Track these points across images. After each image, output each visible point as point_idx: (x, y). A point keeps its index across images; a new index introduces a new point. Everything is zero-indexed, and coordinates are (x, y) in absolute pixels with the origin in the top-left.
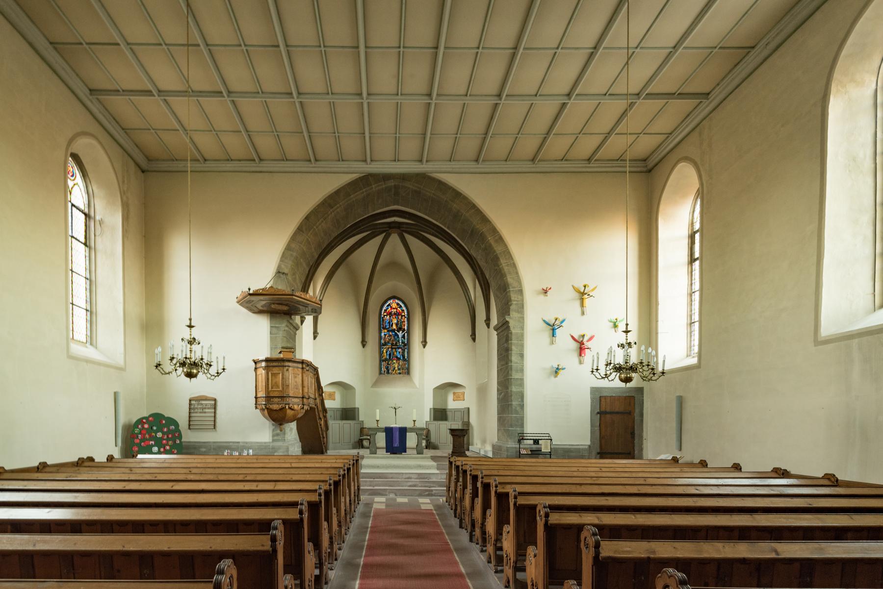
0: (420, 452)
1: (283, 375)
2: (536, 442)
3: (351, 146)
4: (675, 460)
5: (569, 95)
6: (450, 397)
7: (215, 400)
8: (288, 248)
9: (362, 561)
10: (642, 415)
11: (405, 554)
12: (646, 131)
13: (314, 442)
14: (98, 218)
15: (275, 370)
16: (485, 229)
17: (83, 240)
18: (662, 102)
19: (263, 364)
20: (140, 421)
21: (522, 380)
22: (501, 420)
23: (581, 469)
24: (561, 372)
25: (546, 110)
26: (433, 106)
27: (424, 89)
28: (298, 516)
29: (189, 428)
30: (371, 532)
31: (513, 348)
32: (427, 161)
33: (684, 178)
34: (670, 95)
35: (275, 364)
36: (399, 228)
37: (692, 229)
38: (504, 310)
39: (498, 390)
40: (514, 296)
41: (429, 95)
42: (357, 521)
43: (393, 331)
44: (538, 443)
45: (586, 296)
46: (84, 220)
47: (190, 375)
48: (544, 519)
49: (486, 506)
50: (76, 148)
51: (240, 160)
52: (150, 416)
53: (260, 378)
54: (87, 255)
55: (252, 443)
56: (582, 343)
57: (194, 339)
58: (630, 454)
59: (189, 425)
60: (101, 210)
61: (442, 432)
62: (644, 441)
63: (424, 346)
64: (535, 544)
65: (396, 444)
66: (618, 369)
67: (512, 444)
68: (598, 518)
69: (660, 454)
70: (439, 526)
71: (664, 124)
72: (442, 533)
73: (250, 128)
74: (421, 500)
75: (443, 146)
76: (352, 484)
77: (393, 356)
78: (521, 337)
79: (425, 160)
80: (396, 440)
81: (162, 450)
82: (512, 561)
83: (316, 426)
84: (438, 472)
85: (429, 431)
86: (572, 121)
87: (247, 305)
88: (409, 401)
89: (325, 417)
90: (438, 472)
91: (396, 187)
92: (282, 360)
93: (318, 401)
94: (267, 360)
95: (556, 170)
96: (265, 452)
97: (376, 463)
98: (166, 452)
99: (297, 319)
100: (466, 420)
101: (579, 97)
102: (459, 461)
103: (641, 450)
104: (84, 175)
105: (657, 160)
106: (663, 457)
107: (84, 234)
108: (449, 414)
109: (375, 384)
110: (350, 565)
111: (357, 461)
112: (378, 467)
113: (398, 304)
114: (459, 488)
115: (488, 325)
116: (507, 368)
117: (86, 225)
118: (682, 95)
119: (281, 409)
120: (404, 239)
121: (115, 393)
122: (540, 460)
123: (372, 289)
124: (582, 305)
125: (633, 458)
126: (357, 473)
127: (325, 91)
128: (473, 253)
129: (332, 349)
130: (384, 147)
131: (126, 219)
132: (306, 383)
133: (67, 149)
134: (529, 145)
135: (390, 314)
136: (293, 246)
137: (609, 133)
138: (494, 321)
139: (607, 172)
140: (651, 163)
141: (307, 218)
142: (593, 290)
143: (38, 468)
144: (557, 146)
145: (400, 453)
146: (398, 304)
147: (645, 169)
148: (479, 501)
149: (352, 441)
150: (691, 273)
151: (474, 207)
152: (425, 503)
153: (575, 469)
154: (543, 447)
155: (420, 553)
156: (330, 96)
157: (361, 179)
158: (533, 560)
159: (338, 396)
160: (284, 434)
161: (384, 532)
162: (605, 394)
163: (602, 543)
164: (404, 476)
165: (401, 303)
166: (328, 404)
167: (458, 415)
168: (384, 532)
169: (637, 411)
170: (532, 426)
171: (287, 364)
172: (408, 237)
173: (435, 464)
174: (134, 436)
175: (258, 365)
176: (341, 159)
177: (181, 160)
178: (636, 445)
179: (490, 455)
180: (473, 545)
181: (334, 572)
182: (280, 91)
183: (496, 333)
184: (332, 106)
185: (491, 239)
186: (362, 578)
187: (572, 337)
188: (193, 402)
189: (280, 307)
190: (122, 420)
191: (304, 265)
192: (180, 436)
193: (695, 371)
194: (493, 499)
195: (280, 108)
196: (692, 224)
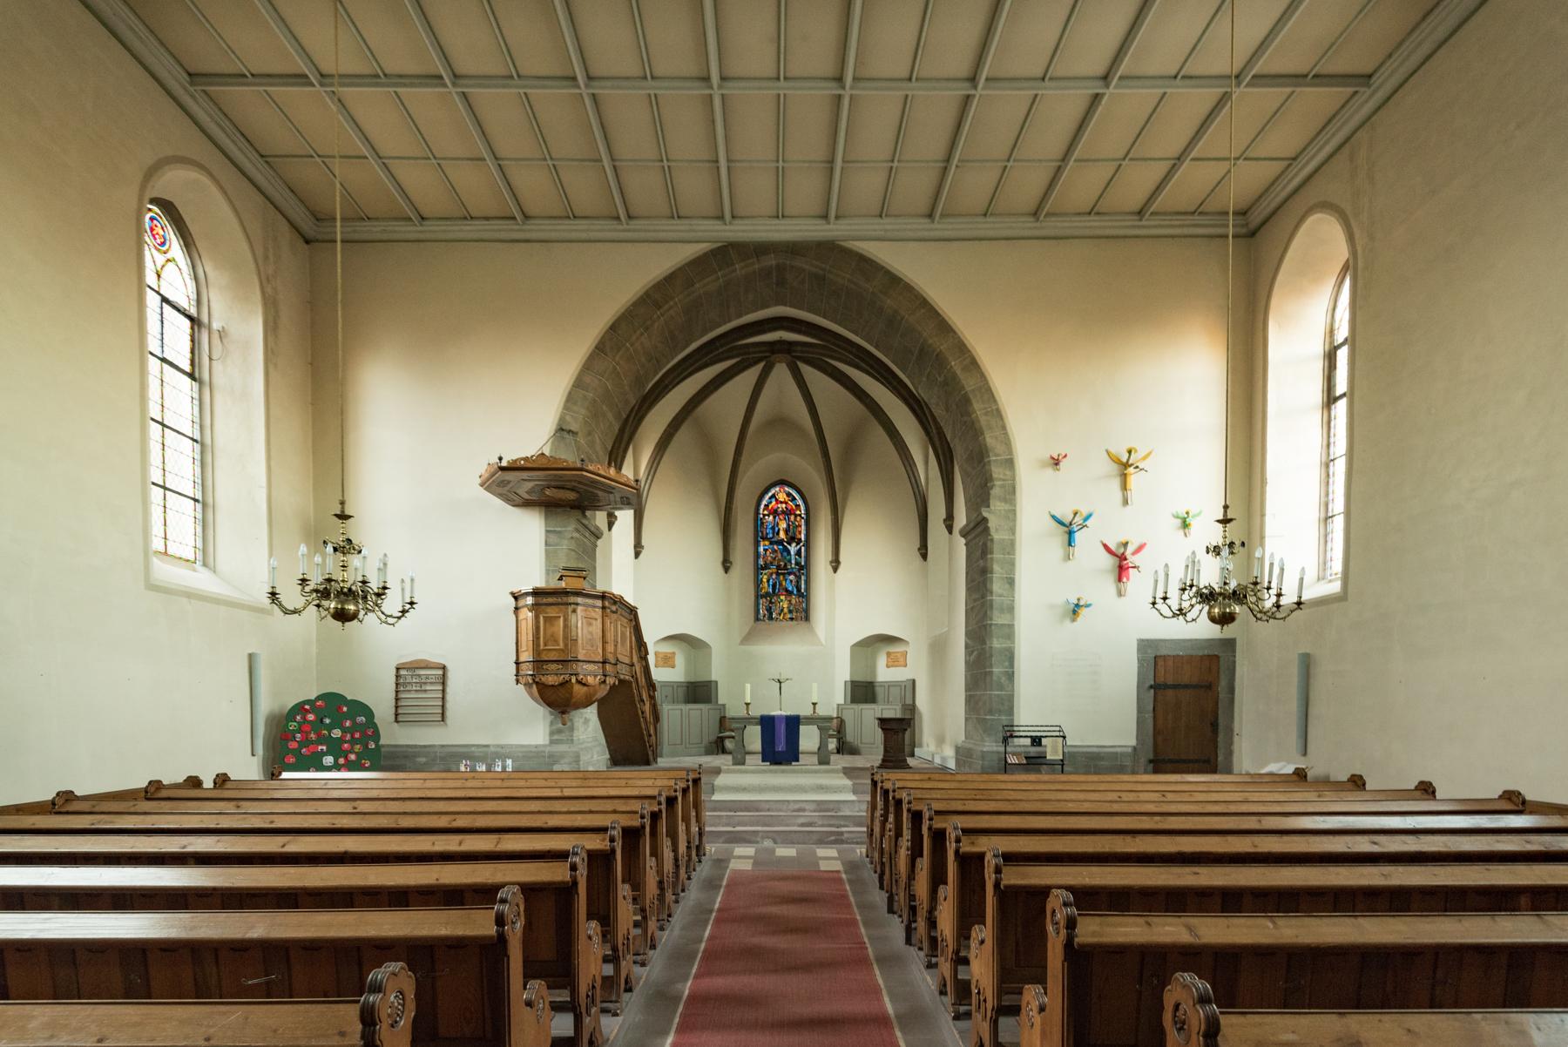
0: (824, 761)
1: (566, 620)
2: (1036, 741)
3: (694, 188)
4: (1300, 775)
5: (1106, 78)
6: (882, 661)
7: (444, 668)
8: (578, 384)
9: (687, 989)
10: (1231, 690)
11: (776, 971)
12: (1249, 154)
13: (631, 741)
14: (216, 325)
15: (552, 612)
16: (943, 346)
17: (188, 368)
18: (1278, 93)
19: (530, 600)
20: (300, 708)
21: (1011, 626)
22: (972, 702)
23: (1125, 796)
24: (1083, 612)
25: (1064, 106)
26: (846, 102)
27: (827, 67)
28: (492, 930)
29: (397, 721)
30: (718, 921)
31: (996, 567)
32: (837, 217)
33: (1322, 239)
34: (1297, 79)
35: (550, 600)
36: (789, 352)
37: (1332, 342)
38: (980, 496)
39: (967, 647)
40: (997, 472)
41: (840, 79)
42: (693, 895)
43: (780, 542)
44: (1040, 744)
45: (1131, 470)
46: (189, 331)
47: (342, 616)
48: (1063, 932)
49: (938, 878)
50: (160, 188)
51: (487, 219)
52: (318, 698)
53: (523, 625)
54: (196, 396)
55: (511, 746)
56: (1123, 558)
57: (349, 541)
58: (1207, 761)
59: (396, 715)
60: (220, 312)
61: (865, 724)
62: (1236, 738)
63: (835, 570)
64: (1041, 979)
65: (781, 746)
66: (1208, 597)
67: (992, 746)
68: (1190, 928)
69: (1266, 764)
70: (849, 905)
71: (1283, 141)
72: (854, 923)
73: (501, 153)
74: (821, 852)
75: (866, 186)
76: (681, 827)
77: (779, 589)
78: (1010, 547)
79: (833, 214)
80: (780, 741)
81: (341, 761)
82: (989, 1006)
83: (635, 717)
84: (853, 797)
85: (842, 722)
86: (1109, 135)
87: (500, 490)
88: (806, 670)
89: (652, 698)
90: (853, 797)
91: (781, 269)
92: (565, 593)
93: (638, 668)
94: (536, 593)
95: (1076, 233)
96: (533, 763)
97: (740, 783)
98: (350, 766)
99: (600, 518)
100: (909, 701)
101: (1124, 83)
102: (892, 779)
103: (1230, 753)
104: (188, 243)
105: (1273, 205)
106: (1273, 767)
107: (189, 355)
108: (879, 691)
109: (748, 638)
110: (662, 998)
111: (696, 781)
112: (744, 789)
113: (789, 495)
114: (890, 834)
115: (950, 529)
116: (983, 605)
117: (193, 341)
118: (1321, 79)
119: (562, 684)
120: (797, 363)
121: (251, 656)
122: (1046, 777)
123: (741, 468)
124: (1124, 487)
125: (1214, 771)
126: (697, 805)
127: (641, 74)
128: (922, 392)
129: (666, 575)
130: (756, 190)
131: (271, 328)
132: (610, 636)
133: (143, 187)
134: (1027, 185)
135: (775, 513)
136: (587, 379)
137: (1180, 159)
138: (961, 519)
139: (1173, 237)
140: (1256, 218)
141: (613, 327)
142: (1145, 458)
143: (53, 803)
144: (1082, 185)
145: (789, 762)
146: (789, 495)
147: (1244, 231)
148: (924, 863)
149: (705, 741)
150: (1328, 424)
151: (924, 304)
152: (829, 858)
153: (1113, 796)
154: (1049, 750)
155: (807, 967)
156: (650, 82)
157: (713, 253)
158: (1037, 1019)
159: (680, 660)
160: (572, 729)
161: (744, 919)
162: (1164, 652)
163: (1223, 1020)
164: (793, 806)
165: (794, 493)
166: (659, 674)
167: (895, 691)
168: (744, 919)
169: (1223, 683)
170: (1029, 714)
171: (572, 599)
172: (808, 371)
173: (848, 783)
174: (286, 736)
175: (521, 603)
176: (676, 215)
177: (377, 219)
178: (1221, 744)
179: (952, 764)
180: (913, 950)
181: (620, 1019)
182: (559, 73)
183: (963, 541)
184: (654, 102)
185: (955, 364)
186: (680, 1030)
187: (1105, 546)
188: (403, 672)
189: (563, 492)
190: (265, 706)
191: (610, 416)
192: (376, 735)
193: (1335, 606)
194: (951, 854)
195: (554, 104)
196: (1331, 332)
